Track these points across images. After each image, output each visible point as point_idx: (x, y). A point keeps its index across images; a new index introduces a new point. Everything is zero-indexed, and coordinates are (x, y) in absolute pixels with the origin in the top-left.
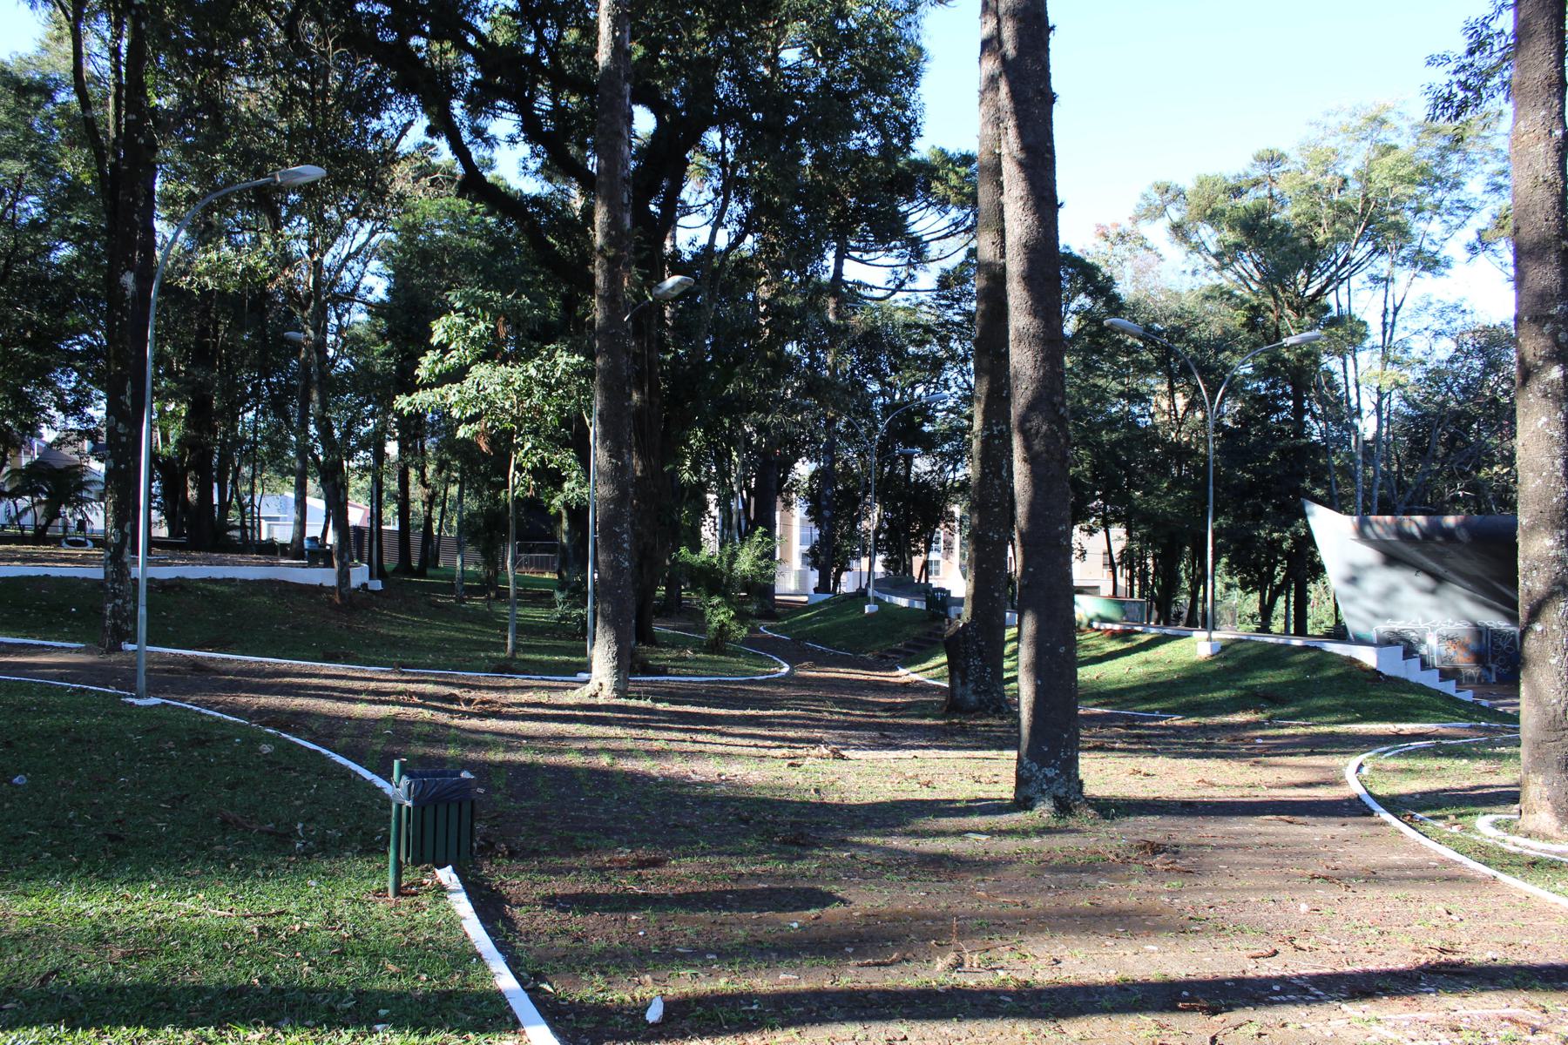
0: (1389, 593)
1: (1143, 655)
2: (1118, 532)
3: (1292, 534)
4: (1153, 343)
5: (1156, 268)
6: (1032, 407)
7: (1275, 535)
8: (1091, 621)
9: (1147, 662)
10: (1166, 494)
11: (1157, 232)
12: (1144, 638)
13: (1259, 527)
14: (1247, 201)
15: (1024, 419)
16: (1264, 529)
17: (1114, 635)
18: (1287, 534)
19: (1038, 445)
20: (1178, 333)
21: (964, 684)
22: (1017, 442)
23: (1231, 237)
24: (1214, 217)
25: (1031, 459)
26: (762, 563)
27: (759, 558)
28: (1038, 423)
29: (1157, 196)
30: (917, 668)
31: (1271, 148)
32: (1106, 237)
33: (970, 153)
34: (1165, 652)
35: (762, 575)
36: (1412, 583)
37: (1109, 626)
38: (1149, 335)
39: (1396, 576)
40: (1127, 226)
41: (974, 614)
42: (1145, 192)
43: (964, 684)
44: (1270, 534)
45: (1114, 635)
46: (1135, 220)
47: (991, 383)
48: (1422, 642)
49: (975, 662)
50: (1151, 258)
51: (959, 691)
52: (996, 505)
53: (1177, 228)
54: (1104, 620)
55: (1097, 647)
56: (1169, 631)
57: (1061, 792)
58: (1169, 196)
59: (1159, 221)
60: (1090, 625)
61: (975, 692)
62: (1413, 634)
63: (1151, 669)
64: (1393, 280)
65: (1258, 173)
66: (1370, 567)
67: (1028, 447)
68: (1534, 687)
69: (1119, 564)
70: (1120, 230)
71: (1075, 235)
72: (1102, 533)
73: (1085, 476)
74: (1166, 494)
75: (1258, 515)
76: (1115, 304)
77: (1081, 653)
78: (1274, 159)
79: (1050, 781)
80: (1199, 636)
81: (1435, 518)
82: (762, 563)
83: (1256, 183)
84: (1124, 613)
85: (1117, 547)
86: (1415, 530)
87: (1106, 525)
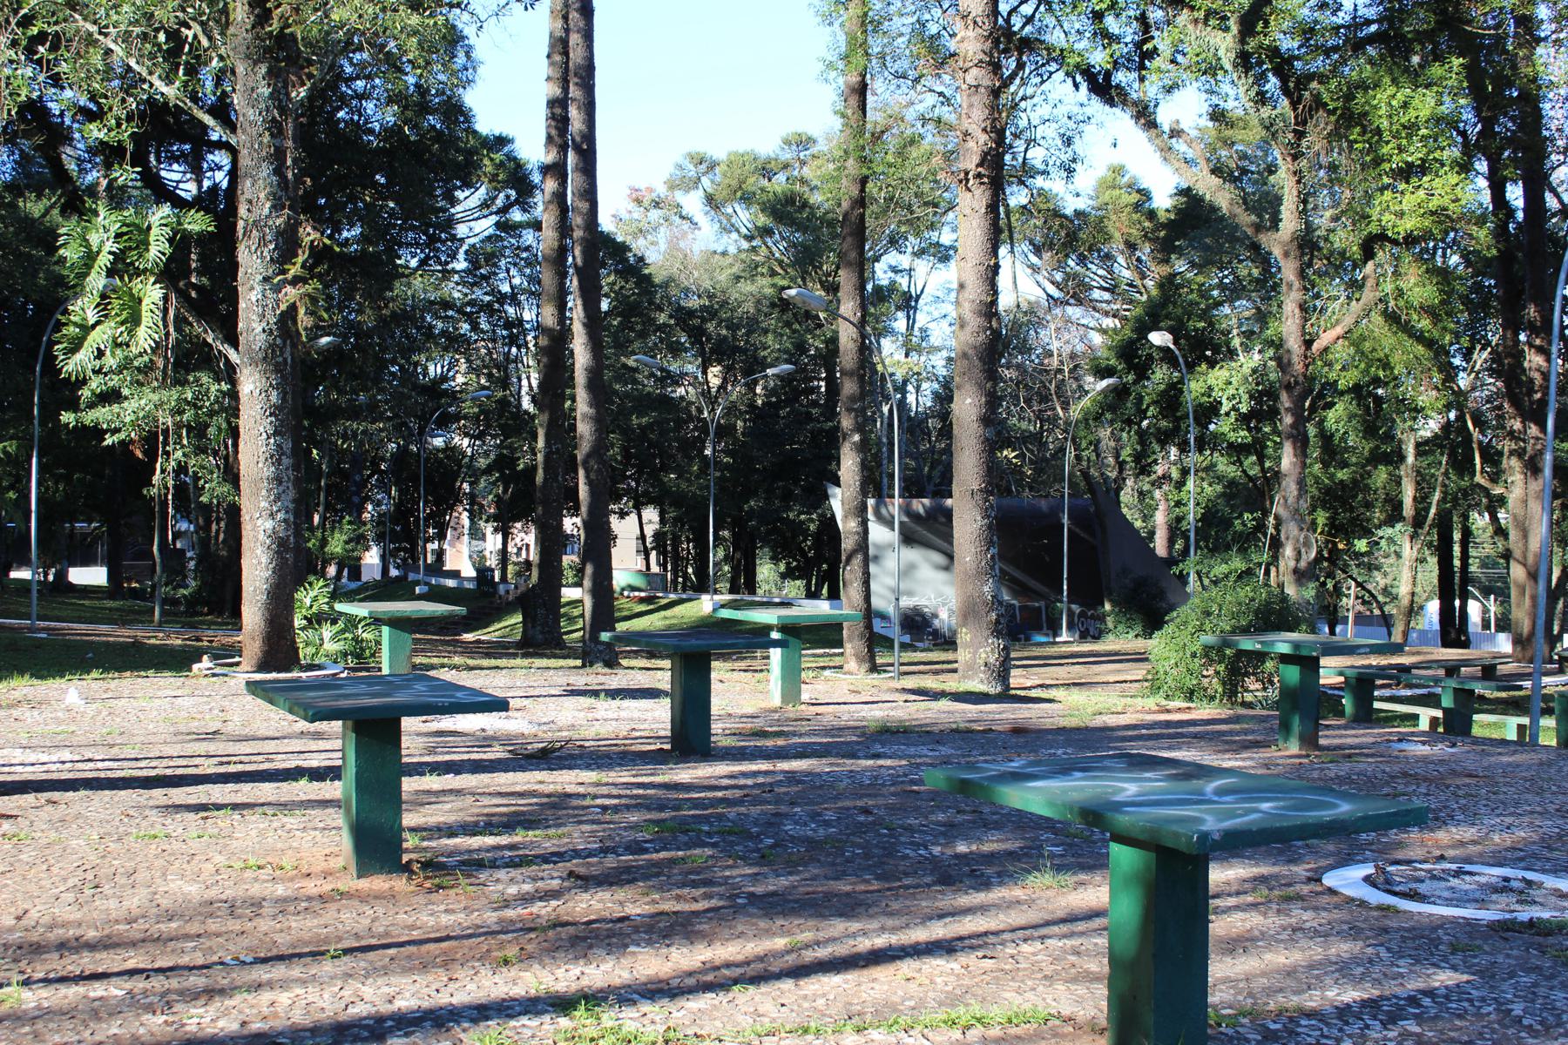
0: (907, 571)
1: (663, 613)
2: (651, 514)
3: (819, 516)
4: (684, 322)
5: (690, 236)
6: (589, 456)
7: (803, 517)
8: (623, 589)
9: (666, 618)
10: (698, 477)
11: (693, 203)
12: (664, 602)
13: (790, 509)
14: (779, 183)
15: (585, 463)
16: (792, 510)
17: (642, 600)
18: (814, 516)
19: (593, 476)
20: (710, 313)
21: (533, 627)
22: (581, 473)
23: (763, 220)
24: (747, 199)
25: (590, 482)
26: (349, 547)
27: (347, 543)
28: (592, 462)
29: (691, 167)
30: (479, 632)
31: (799, 131)
32: (639, 201)
33: (504, 135)
34: (678, 610)
35: (349, 557)
36: (928, 560)
37: (637, 594)
38: (683, 316)
39: (913, 555)
40: (662, 190)
41: (540, 578)
42: (680, 162)
43: (533, 627)
44: (798, 515)
45: (642, 600)
46: (672, 186)
47: (551, 415)
48: (935, 616)
49: (541, 612)
50: (686, 225)
51: (530, 632)
52: (554, 501)
53: (710, 199)
54: (633, 588)
55: (629, 609)
56: (684, 596)
57: (607, 658)
58: (703, 167)
59: (692, 192)
60: (622, 594)
61: (542, 633)
62: (926, 610)
63: (667, 622)
64: (622, 518)
65: (787, 155)
66: (890, 546)
67: (587, 477)
68: (849, 598)
69: (652, 549)
70: (654, 195)
71: (613, 214)
72: (633, 517)
73: (616, 460)
74: (698, 477)
75: (787, 497)
76: (645, 282)
77: (617, 614)
78: (803, 142)
79: (601, 652)
80: (705, 598)
81: (938, 500)
82: (349, 547)
83: (786, 166)
84: (649, 583)
85: (649, 531)
86: (921, 511)
87: (638, 508)
